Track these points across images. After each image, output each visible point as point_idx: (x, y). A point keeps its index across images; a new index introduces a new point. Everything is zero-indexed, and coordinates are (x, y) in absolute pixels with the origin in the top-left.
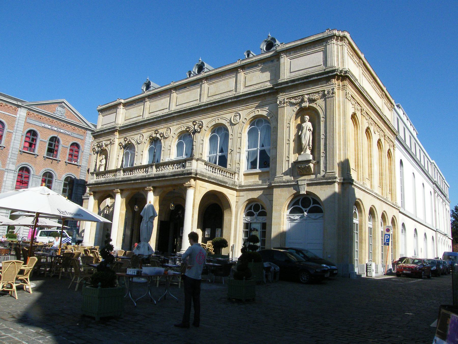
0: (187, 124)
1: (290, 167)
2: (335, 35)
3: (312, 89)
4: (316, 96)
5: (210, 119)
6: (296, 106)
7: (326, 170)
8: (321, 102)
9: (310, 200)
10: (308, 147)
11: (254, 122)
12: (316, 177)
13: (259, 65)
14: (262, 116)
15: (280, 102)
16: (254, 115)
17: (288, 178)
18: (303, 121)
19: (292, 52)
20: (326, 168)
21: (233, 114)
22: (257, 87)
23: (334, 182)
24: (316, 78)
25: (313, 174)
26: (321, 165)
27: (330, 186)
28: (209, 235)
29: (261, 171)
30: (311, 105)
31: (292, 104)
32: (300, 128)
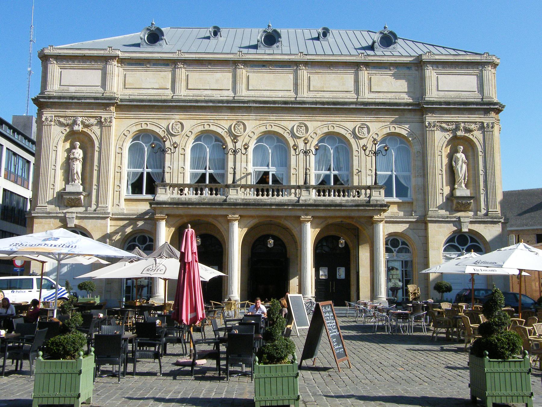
0: (276, 122)
1: (55, 196)
2: (118, 56)
3: (468, 117)
4: (93, 121)
5: (319, 123)
6: (448, 133)
7: (98, 205)
8: (96, 129)
9: (467, 238)
10: (463, 181)
11: (201, 137)
12: (86, 210)
13: (392, 68)
14: (399, 135)
15: (429, 123)
16: (327, 131)
17: (443, 212)
18: (73, 147)
19: (439, 66)
20: (97, 202)
21: (297, 123)
22: (389, 95)
23: (108, 217)
24: (475, 107)
25: (82, 206)
26: (482, 203)
27: (494, 225)
28: (325, 275)
29: (401, 201)
30: (467, 135)
31: (61, 124)
32: (451, 157)
